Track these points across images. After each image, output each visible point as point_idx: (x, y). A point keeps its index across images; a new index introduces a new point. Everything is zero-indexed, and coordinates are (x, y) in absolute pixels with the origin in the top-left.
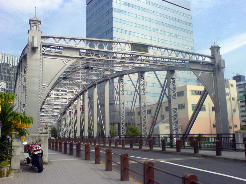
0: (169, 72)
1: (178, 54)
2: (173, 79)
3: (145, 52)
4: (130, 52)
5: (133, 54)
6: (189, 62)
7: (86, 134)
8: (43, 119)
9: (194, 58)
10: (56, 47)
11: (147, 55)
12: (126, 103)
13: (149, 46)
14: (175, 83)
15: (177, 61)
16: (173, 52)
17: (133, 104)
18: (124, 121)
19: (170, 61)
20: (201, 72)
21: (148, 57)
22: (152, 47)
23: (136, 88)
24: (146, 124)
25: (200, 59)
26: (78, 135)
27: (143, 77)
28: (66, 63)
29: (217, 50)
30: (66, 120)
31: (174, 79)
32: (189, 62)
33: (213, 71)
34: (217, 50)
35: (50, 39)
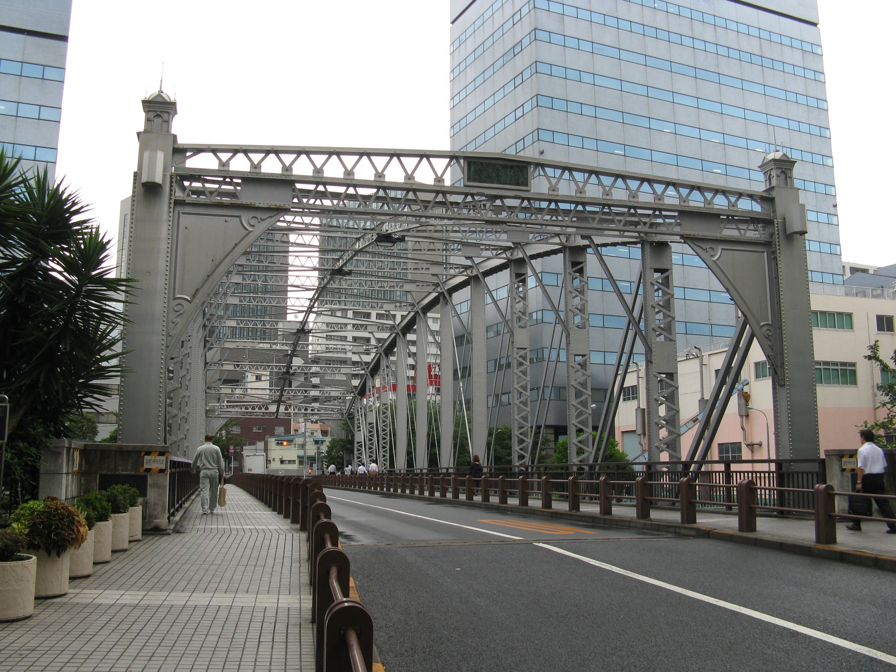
0: (648, 248)
1: (586, 182)
2: (662, 271)
3: (518, 184)
4: (465, 186)
5: (475, 191)
6: (676, 214)
7: (447, 460)
8: (316, 411)
9: (696, 201)
10: (651, 212)
11: (523, 194)
12: (596, 358)
13: (530, 163)
14: (668, 287)
15: (411, 196)
16: (617, 185)
17: (623, 362)
18: (525, 419)
19: (354, 192)
20: (720, 248)
21: (529, 199)
22: (543, 166)
23: (630, 312)
24: (587, 427)
25: (720, 202)
26: (421, 462)
27: (579, 267)
28: (250, 229)
29: (783, 172)
30: (369, 414)
31: (667, 270)
32: (676, 214)
33: (768, 244)
34: (783, 172)
35: (202, 155)
